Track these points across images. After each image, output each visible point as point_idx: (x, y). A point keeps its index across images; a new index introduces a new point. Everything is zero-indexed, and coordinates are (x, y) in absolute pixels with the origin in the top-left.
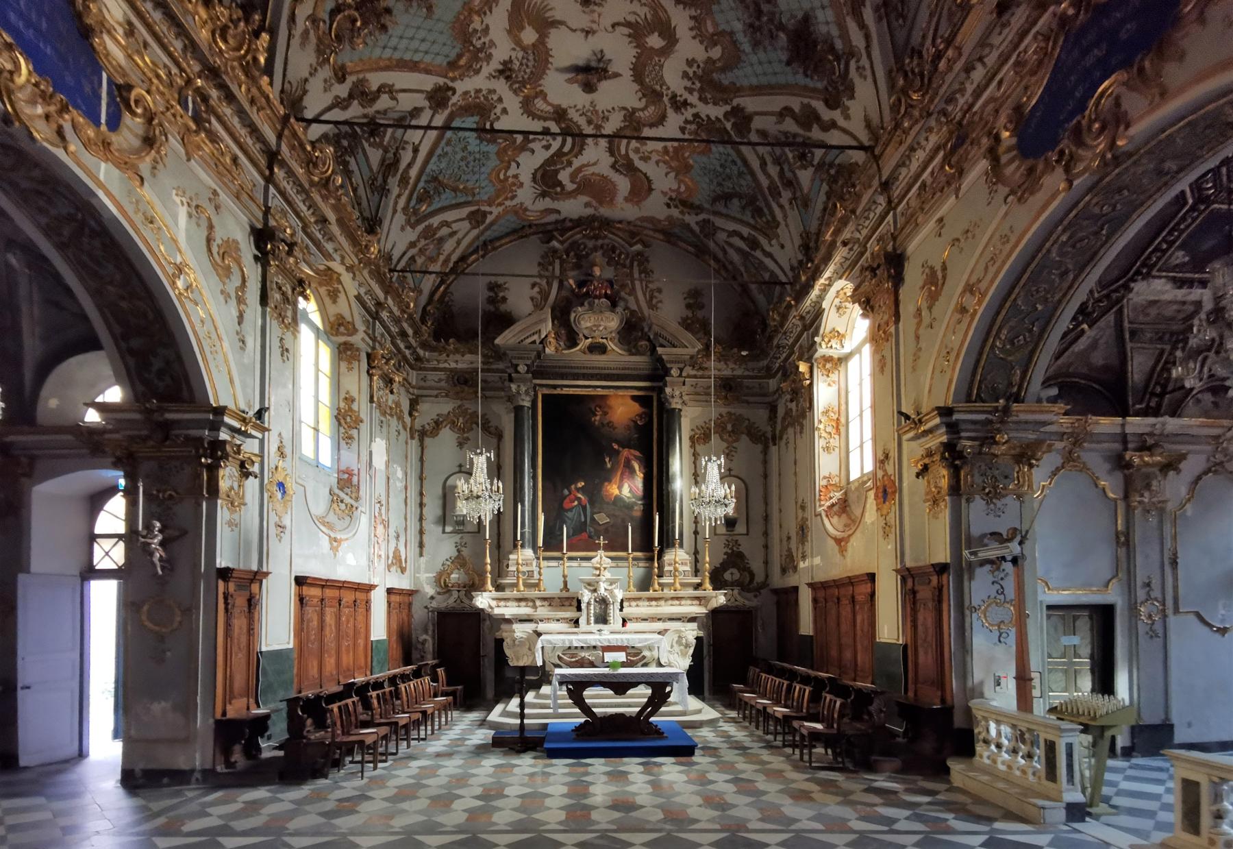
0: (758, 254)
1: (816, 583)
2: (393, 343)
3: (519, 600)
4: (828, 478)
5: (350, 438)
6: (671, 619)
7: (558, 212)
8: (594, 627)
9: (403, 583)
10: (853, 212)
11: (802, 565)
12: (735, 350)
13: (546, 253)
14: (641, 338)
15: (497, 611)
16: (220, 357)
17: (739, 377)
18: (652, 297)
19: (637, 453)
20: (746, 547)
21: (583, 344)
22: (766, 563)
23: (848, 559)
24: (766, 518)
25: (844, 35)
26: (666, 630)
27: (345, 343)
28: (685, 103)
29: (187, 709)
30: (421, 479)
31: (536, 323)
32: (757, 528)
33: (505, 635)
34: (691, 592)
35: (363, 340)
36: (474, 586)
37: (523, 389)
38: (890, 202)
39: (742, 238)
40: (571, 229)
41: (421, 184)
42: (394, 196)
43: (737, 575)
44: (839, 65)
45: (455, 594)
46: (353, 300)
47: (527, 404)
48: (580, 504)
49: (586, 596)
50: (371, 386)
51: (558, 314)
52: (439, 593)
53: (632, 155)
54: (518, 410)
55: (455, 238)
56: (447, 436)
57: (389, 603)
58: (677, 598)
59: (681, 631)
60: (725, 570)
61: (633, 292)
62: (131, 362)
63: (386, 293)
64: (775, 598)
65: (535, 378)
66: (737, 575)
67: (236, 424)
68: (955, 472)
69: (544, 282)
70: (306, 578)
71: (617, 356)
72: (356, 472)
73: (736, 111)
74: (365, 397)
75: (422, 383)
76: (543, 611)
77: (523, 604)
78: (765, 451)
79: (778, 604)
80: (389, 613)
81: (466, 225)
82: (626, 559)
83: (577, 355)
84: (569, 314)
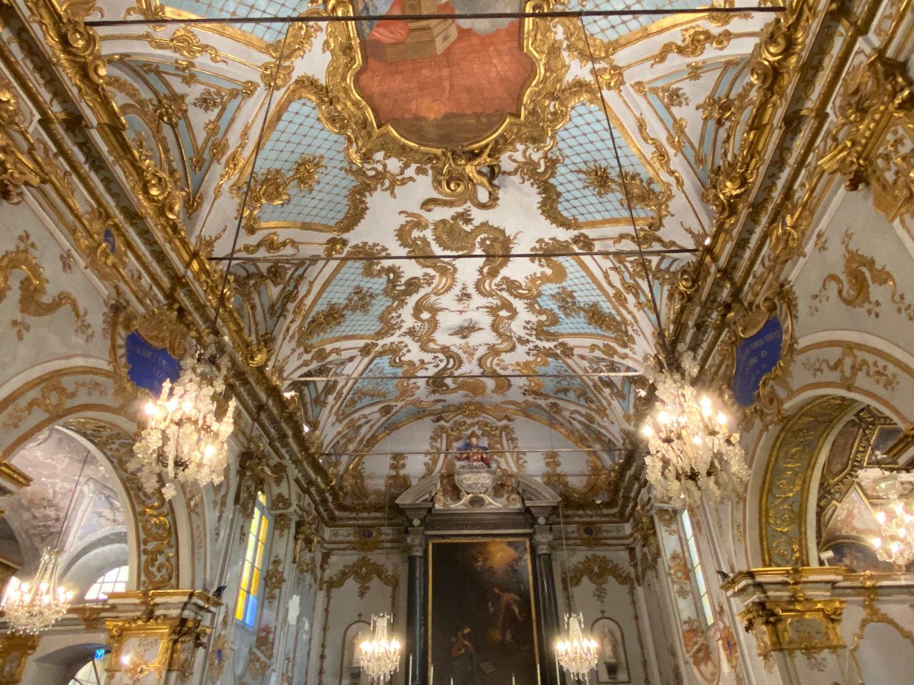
2: (317, 510)
5: (272, 597)
16: (202, 550)
18: (518, 459)
25: (619, 313)
27: (281, 515)
28: (528, 341)
39: (582, 415)
41: (350, 396)
50: (295, 548)
54: (412, 560)
56: (351, 584)
67: (201, 603)
73: (562, 344)
74: (289, 558)
75: (334, 539)
78: (632, 593)
81: (377, 416)
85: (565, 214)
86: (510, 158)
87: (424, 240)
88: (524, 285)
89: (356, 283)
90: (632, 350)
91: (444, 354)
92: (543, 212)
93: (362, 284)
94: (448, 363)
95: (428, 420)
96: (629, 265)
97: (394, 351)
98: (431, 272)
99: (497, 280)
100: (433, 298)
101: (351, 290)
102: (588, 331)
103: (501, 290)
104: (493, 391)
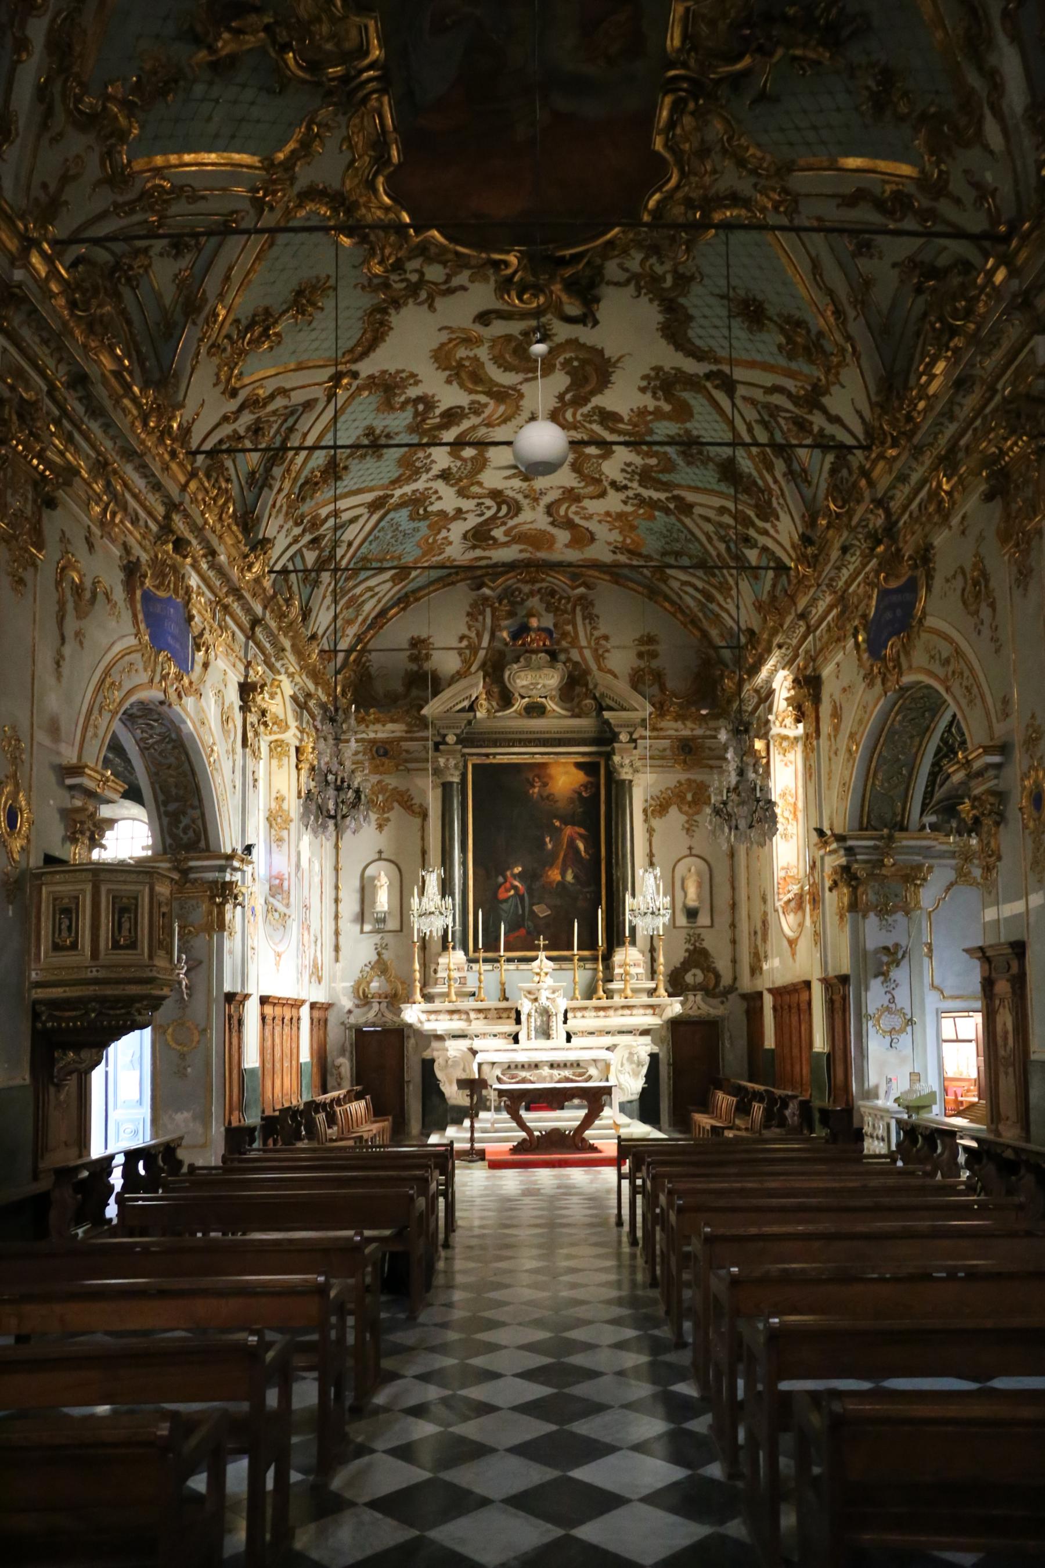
0: (713, 606)
3: (452, 1012)
4: (786, 869)
5: (280, 840)
9: (320, 996)
10: (782, 626)
13: (476, 601)
14: (586, 696)
17: (699, 737)
19: (582, 831)
20: (708, 943)
21: (519, 704)
22: (734, 961)
24: (734, 906)
26: (615, 1046)
28: (626, 487)
29: (205, 1118)
30: (337, 870)
31: (466, 688)
32: (723, 919)
33: (436, 1054)
34: (645, 999)
36: (395, 999)
37: (452, 762)
38: (808, 627)
39: (696, 589)
40: (502, 574)
43: (700, 977)
45: (376, 1007)
46: (288, 699)
49: (526, 1007)
51: (490, 670)
52: (357, 1006)
53: (571, 515)
57: (312, 1019)
58: (628, 1007)
60: (687, 971)
61: (574, 643)
62: (166, 821)
63: (317, 684)
64: (745, 1005)
65: (465, 747)
68: (855, 889)
69: (473, 635)
70: (268, 997)
71: (557, 719)
76: (478, 1025)
77: (456, 1016)
79: (748, 1012)
80: (312, 1030)
82: (570, 959)
83: (511, 719)
84: (502, 671)
85: (698, 342)
86: (621, 266)
87: (476, 359)
88: (626, 418)
89: (367, 423)
90: (774, 526)
92: (662, 330)
93: (375, 424)
94: (499, 510)
95: (462, 587)
96: (782, 422)
97: (417, 503)
98: (483, 399)
99: (585, 410)
100: (483, 430)
101: (360, 432)
102: (715, 487)
103: (590, 422)
104: (566, 546)
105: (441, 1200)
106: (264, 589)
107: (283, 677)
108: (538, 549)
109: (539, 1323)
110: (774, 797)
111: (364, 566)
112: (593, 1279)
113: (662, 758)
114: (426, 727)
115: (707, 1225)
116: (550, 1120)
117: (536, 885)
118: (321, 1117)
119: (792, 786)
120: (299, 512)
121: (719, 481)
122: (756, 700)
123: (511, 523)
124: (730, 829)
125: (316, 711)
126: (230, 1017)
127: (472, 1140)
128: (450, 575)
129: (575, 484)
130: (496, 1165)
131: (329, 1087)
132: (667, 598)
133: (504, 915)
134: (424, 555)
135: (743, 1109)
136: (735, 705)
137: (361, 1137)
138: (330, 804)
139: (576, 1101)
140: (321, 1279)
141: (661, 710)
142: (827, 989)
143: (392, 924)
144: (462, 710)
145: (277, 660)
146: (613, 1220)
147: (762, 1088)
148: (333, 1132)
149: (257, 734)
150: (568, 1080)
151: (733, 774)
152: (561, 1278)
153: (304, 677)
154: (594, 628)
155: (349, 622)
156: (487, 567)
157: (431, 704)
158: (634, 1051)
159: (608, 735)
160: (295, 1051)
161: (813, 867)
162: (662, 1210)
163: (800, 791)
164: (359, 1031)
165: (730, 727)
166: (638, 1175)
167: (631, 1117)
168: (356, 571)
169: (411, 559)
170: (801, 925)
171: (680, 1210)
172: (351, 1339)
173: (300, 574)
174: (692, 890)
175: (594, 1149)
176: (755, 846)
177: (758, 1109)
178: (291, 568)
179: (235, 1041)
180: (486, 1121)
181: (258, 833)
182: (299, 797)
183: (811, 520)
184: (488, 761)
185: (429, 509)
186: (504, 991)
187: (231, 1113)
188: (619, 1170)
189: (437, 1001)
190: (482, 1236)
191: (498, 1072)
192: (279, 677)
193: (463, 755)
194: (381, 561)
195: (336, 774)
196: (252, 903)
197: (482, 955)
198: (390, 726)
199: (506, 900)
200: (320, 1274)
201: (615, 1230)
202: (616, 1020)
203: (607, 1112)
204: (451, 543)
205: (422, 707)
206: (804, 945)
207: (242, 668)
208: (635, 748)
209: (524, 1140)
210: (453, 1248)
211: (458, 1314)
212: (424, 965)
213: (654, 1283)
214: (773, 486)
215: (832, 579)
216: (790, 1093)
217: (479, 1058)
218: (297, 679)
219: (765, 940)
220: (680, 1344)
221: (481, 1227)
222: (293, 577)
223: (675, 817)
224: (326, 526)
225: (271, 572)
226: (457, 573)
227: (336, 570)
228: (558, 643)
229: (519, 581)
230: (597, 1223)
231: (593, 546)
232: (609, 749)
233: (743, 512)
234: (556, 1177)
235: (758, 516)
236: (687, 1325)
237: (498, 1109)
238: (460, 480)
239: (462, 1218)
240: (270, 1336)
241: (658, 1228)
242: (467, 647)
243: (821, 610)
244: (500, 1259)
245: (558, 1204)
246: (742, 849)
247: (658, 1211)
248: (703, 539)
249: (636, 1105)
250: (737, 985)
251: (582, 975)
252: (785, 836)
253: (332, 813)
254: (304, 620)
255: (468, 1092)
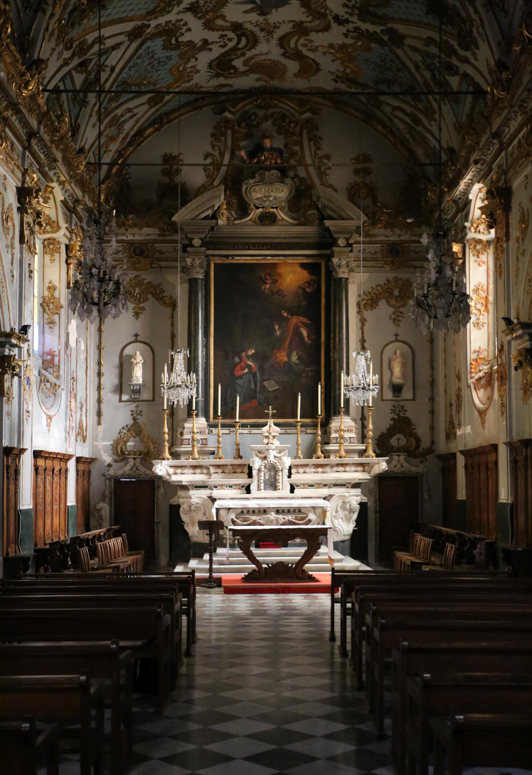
0: (419, 128)
1: (468, 451)
3: (195, 467)
4: (478, 352)
5: (52, 323)
6: (336, 485)
7: (231, 86)
8: (264, 493)
9: (84, 452)
10: (478, 144)
11: (459, 433)
12: (401, 219)
15: (174, 478)
17: (405, 242)
19: (306, 320)
21: (254, 214)
22: (432, 428)
23: (486, 431)
24: (433, 383)
25: (465, 9)
26: (331, 496)
28: (347, 21)
30: (99, 348)
33: (181, 501)
34: (356, 459)
35: (65, 235)
36: (149, 455)
37: (198, 262)
38: (501, 144)
39: (405, 113)
42: (91, 106)
43: (403, 441)
44: (465, 26)
47: (201, 276)
48: (250, 371)
49: (257, 463)
51: (230, 184)
52: (116, 461)
53: (300, 48)
55: (135, 118)
57: (77, 471)
58: (342, 465)
59: (345, 497)
60: (392, 436)
61: (301, 162)
63: (84, 192)
65: (208, 249)
66: (403, 441)
69: (216, 153)
71: (286, 226)
72: (57, 353)
73: (391, 31)
76: (216, 478)
77: (198, 471)
80: (77, 480)
82: (293, 426)
83: (247, 225)
90: (474, 55)
91: (234, 31)
94: (239, 42)
97: (170, 32)
104: (296, 75)
105: (184, 617)
106: (39, 106)
107: (55, 185)
108: (272, 78)
109: (264, 718)
110: (469, 291)
111: (124, 89)
112: (310, 683)
113: (373, 260)
114: (176, 231)
115: (405, 639)
116: (276, 553)
117: (267, 365)
118: (85, 550)
119: (484, 282)
120: (68, 37)
121: (427, 13)
122: (454, 210)
123: (249, 54)
124: (430, 317)
125: (84, 215)
126: (8, 467)
127: (211, 570)
128: (197, 100)
129: (303, 18)
130: (230, 590)
131: (91, 526)
132: (380, 122)
133: (239, 389)
134: (176, 81)
135: (438, 548)
136: (436, 215)
137: (118, 567)
138: (93, 294)
139: (298, 540)
140: (83, 678)
141: (373, 218)
142: (511, 451)
143: (146, 395)
144: (206, 218)
145: (50, 169)
146: (327, 636)
147: (454, 531)
148: (94, 562)
149: (32, 232)
150: (291, 523)
151: (433, 272)
152: (283, 682)
153: (73, 185)
154: (318, 149)
155: (112, 139)
156: (228, 93)
157: (180, 212)
158: (347, 500)
159: (329, 240)
160: (63, 496)
161: (501, 350)
162: (368, 627)
163: (491, 286)
164: (117, 481)
165: (431, 232)
166: (349, 600)
167: (344, 554)
168: (118, 94)
169: (165, 85)
170: (490, 399)
171: (383, 628)
172: (108, 728)
173: (70, 94)
174: (397, 370)
175: (312, 579)
176: (451, 332)
177: (450, 549)
178: (62, 88)
179: (12, 487)
180: (223, 555)
181: (33, 316)
182: (68, 287)
183: (506, 46)
184: (227, 262)
185: (180, 39)
186: (238, 450)
187: (8, 546)
188: (333, 596)
189: (182, 458)
190: (219, 647)
191: (233, 516)
192: (52, 185)
193: (207, 256)
194: (138, 85)
195: (99, 268)
196: (28, 374)
197: (220, 421)
198: (145, 230)
199: (241, 377)
200: (82, 674)
201: (329, 643)
202: (332, 476)
203: (323, 549)
204: (198, 71)
205: (173, 215)
206: (491, 415)
207: (20, 175)
208: (351, 251)
209: (254, 571)
210: (194, 656)
211: (197, 709)
212: (172, 429)
213: (360, 687)
214: (475, 17)
215: (523, 101)
216: (478, 536)
217: (217, 504)
218: (67, 186)
219: (459, 411)
220: (381, 737)
221: (218, 640)
222: (64, 96)
223: (384, 309)
224: (92, 51)
225: (44, 90)
226: (203, 99)
227: (100, 92)
228: (287, 161)
229: (256, 106)
230: (315, 638)
231: (319, 74)
232: (329, 252)
233: (447, 41)
234: (280, 601)
235: (460, 45)
236: (388, 722)
237: (232, 546)
238: (207, 12)
239: (200, 632)
240: (40, 725)
241: (364, 643)
242: (211, 164)
243: (513, 129)
244: (234, 665)
245: (281, 622)
246: (440, 335)
247: (364, 629)
248: (412, 68)
249: (347, 544)
250: (435, 447)
251: (303, 439)
252: (477, 325)
253: (96, 300)
254: (73, 135)
255: (207, 531)
